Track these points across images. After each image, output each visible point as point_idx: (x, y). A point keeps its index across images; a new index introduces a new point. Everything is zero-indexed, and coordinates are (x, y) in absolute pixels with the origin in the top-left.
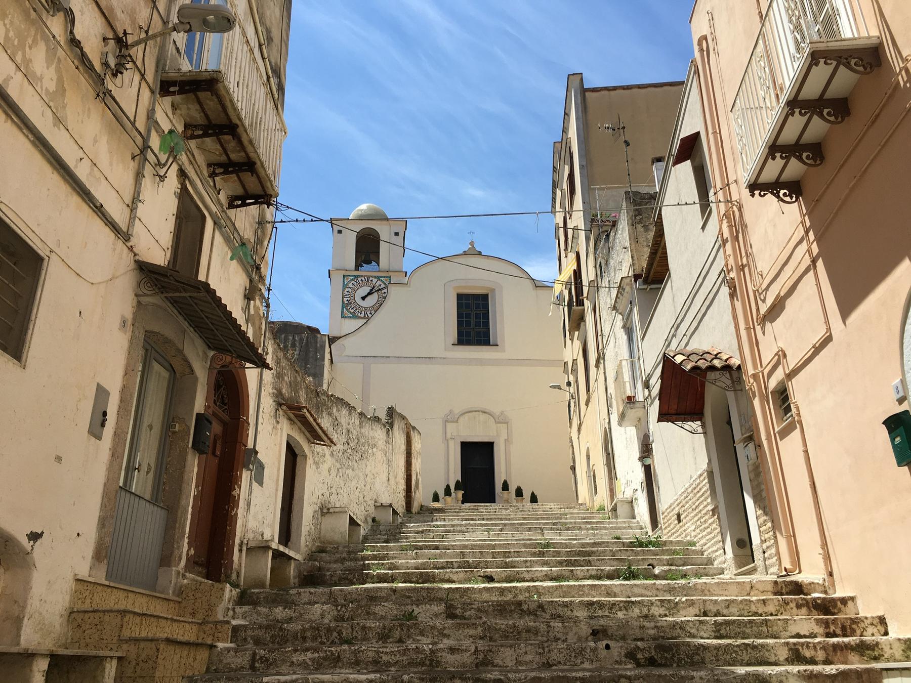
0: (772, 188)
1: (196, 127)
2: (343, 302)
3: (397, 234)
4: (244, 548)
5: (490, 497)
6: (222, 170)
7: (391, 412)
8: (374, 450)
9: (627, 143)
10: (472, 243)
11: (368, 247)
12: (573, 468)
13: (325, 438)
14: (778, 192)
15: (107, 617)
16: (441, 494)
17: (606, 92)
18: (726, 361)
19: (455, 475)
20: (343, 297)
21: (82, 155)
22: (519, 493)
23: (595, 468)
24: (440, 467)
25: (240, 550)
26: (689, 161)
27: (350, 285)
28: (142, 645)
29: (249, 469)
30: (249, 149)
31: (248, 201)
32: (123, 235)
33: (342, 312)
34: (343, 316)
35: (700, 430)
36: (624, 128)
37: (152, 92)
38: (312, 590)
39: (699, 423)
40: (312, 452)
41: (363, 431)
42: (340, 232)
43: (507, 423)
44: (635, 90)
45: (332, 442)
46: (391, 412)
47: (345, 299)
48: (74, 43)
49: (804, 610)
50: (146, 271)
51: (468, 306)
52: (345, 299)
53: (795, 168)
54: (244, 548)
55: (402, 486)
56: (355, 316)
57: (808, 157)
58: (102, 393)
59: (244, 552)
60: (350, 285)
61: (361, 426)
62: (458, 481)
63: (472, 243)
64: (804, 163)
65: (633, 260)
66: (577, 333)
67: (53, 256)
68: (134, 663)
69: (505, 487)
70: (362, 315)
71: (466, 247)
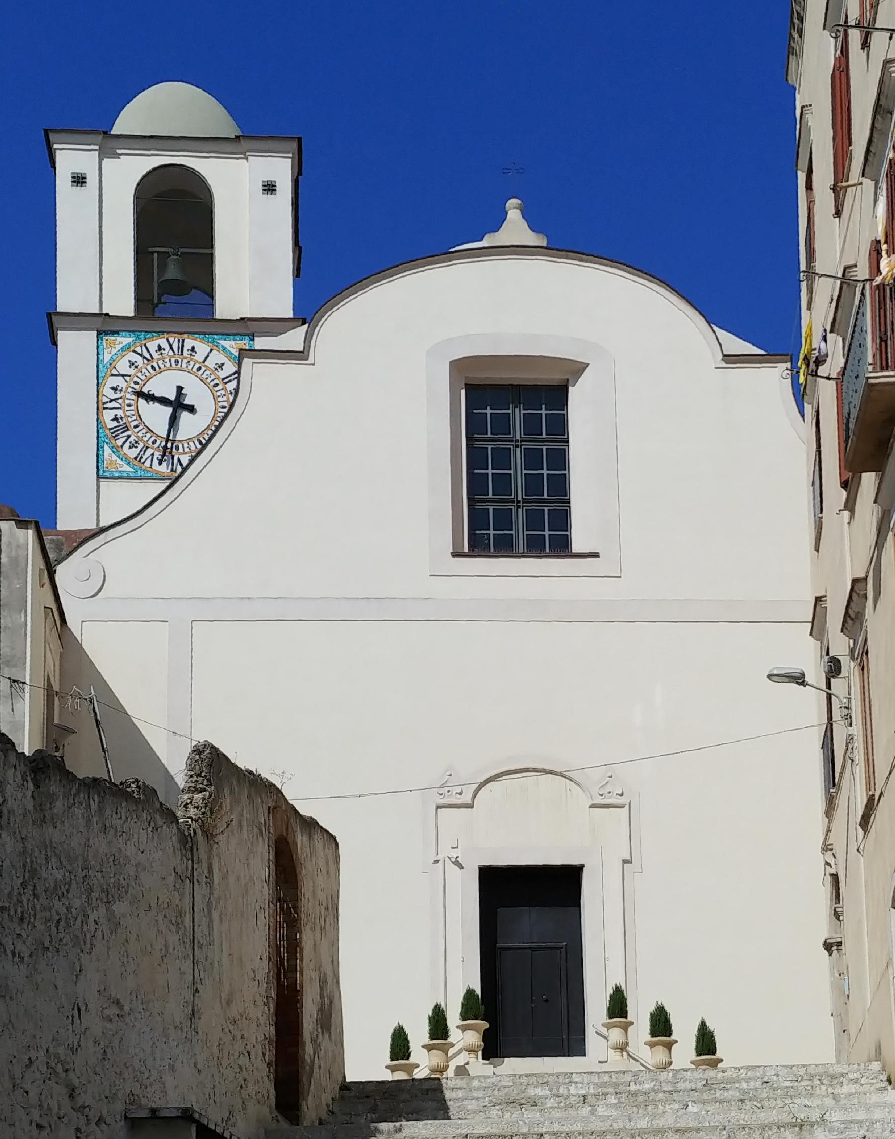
3: (270, 188)
8: (120, 907)
16: (418, 1035)
20: (100, 408)
22: (661, 1024)
38: (280, 1118)
43: (725, 356)
51: (534, 521)
52: (108, 416)
55: (259, 1025)
60: (123, 366)
61: (42, 815)
62: (470, 993)
66: (868, 479)
69: (618, 1006)
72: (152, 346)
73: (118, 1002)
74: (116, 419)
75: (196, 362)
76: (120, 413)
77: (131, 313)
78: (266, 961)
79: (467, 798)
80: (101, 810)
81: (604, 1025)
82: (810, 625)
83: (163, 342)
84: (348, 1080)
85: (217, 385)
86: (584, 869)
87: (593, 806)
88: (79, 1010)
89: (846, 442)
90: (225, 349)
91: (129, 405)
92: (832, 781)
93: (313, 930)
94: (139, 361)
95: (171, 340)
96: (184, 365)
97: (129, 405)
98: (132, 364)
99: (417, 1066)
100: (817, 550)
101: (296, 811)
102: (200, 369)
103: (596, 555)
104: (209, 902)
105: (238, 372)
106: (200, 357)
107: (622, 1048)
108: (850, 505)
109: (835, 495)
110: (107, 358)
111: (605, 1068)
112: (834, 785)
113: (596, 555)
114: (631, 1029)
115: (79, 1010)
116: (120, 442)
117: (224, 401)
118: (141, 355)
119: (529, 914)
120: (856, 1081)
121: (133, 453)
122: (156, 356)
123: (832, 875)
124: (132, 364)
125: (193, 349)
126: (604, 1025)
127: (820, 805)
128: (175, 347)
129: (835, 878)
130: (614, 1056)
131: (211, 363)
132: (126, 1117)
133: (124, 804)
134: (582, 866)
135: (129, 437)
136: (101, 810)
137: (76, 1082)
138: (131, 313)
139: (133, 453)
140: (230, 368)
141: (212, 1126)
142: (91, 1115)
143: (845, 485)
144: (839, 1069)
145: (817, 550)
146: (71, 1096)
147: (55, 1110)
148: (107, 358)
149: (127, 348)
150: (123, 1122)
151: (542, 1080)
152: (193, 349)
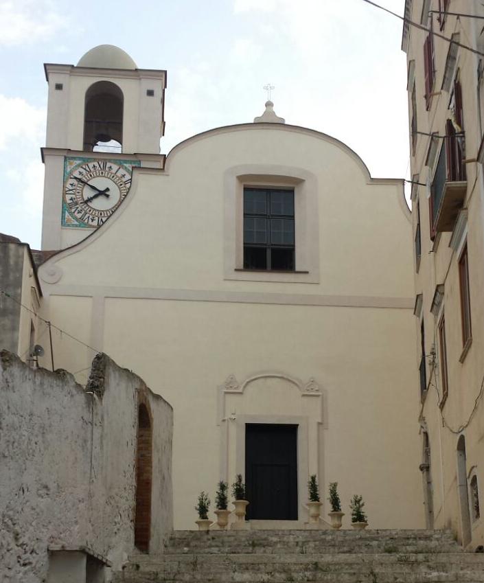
2: (64, 200)
3: (150, 93)
7: (101, 364)
10: (269, 104)
11: (104, 110)
20: (65, 193)
24: (200, 463)
33: (63, 217)
34: (64, 223)
41: (363, 547)
42: (59, 87)
46: (101, 364)
47: (68, 197)
49: (310, 480)
56: (82, 223)
63: (269, 104)
71: (257, 112)
72: (91, 165)
73: (46, 487)
74: (71, 199)
75: (112, 173)
76: (74, 196)
77: (81, 149)
78: (132, 467)
79: (240, 391)
80: (42, 384)
81: (308, 505)
82: (413, 310)
83: (96, 164)
84: (174, 529)
85: (121, 185)
86: (299, 427)
87: (304, 395)
88: (23, 491)
89: (433, 221)
90: (126, 168)
91: (78, 193)
92: (424, 387)
93: (158, 451)
94: (84, 172)
95: (100, 163)
96: (106, 175)
97: (78, 193)
98: (80, 173)
99: (212, 522)
100: (417, 272)
101: (151, 391)
102: (113, 177)
103: (307, 272)
104: (102, 436)
105: (131, 179)
106: (114, 171)
107: (316, 517)
108: (435, 250)
109: (427, 243)
110: (69, 170)
111: (308, 527)
112: (425, 388)
113: (307, 272)
114: (321, 507)
115: (23, 491)
116: (73, 210)
117: (124, 192)
118: (85, 169)
119: (271, 455)
120: (437, 539)
121: (79, 216)
122: (92, 170)
123: (424, 433)
124: (80, 173)
125: (110, 167)
126: (308, 505)
127: (419, 398)
128: (102, 166)
129: (426, 434)
130: (312, 521)
131: (119, 174)
132: (48, 550)
133: (55, 382)
134: (298, 425)
135: (77, 208)
136: (42, 384)
137: (20, 531)
138: (81, 149)
139: (79, 216)
140: (128, 177)
141: (96, 556)
142: (27, 548)
143: (433, 239)
144: (428, 533)
145: (417, 272)
146: (16, 539)
147: (5, 546)
148: (69, 170)
149: (79, 166)
150: (46, 553)
151: (275, 533)
152: (110, 167)
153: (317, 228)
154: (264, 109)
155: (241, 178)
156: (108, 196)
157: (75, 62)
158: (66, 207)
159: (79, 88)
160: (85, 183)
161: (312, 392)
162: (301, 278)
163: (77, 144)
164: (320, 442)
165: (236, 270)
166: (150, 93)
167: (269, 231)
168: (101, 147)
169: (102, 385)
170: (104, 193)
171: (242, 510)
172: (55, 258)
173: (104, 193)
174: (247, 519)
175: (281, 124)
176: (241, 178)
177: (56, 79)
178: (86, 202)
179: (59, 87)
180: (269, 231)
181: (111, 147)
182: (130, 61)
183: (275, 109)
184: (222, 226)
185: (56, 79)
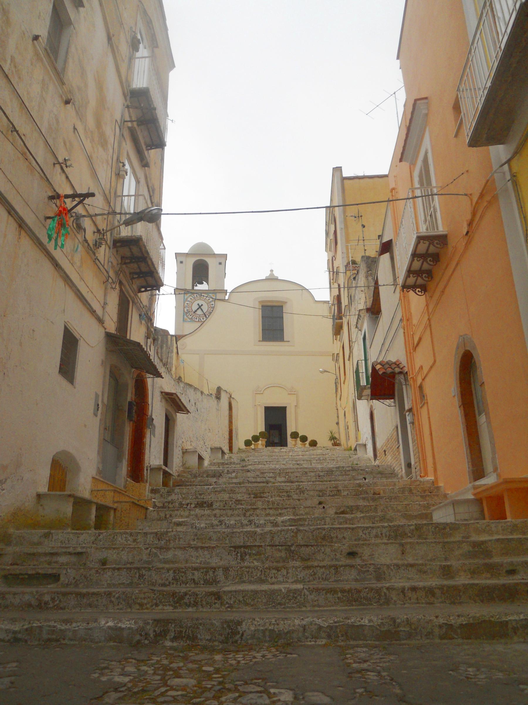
0: (413, 287)
1: (127, 258)
2: (184, 310)
3: (220, 264)
4: (149, 469)
5: (283, 443)
6: (136, 276)
9: (364, 226)
10: (272, 271)
12: (338, 423)
13: (184, 408)
14: (416, 290)
15: (107, 493)
17: (357, 180)
18: (402, 369)
19: (261, 427)
20: (184, 308)
21: (88, 290)
23: (348, 424)
24: (251, 424)
25: (147, 470)
26: (388, 253)
27: (189, 299)
28: (123, 504)
29: (150, 428)
30: (151, 266)
31: (148, 289)
32: (101, 321)
33: (184, 318)
34: (184, 320)
35: (393, 404)
36: (361, 216)
37: (110, 248)
39: (392, 400)
40: (180, 417)
42: (181, 262)
44: (376, 179)
45: (189, 412)
46: (219, 390)
47: (186, 309)
48: (86, 241)
50: (108, 335)
53: (420, 281)
54: (149, 469)
57: (425, 277)
58: (97, 396)
59: (149, 471)
60: (189, 299)
63: (272, 271)
64: (423, 279)
65: (366, 299)
67: (82, 339)
68: (120, 511)
70: (197, 320)
71: (267, 274)
121: (190, 317)
153: (292, 324)
154: (270, 273)
155: (259, 302)
156: (202, 305)
157: (186, 251)
158: (186, 313)
159: (190, 263)
160: (204, 314)
161: (292, 392)
162: (286, 343)
163: (189, 287)
164: (296, 413)
165: (259, 341)
166: (220, 264)
167: (273, 322)
168: (199, 287)
169: (220, 396)
170: (200, 307)
171: (264, 443)
172: (184, 338)
173: (200, 307)
174: (266, 447)
175: (276, 279)
176: (259, 302)
177: (180, 259)
178: (194, 312)
179: (181, 262)
180: (273, 322)
181: (204, 287)
182: (213, 251)
183: (274, 272)
184: (252, 322)
185: (180, 259)
